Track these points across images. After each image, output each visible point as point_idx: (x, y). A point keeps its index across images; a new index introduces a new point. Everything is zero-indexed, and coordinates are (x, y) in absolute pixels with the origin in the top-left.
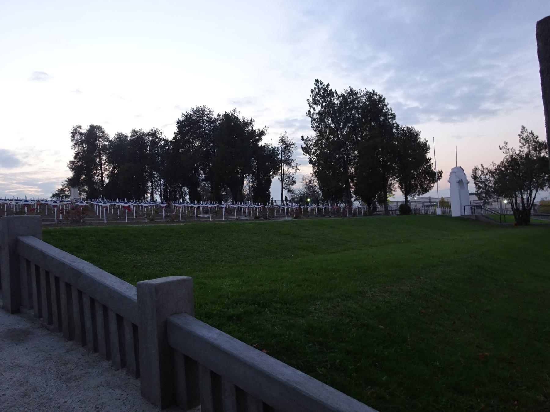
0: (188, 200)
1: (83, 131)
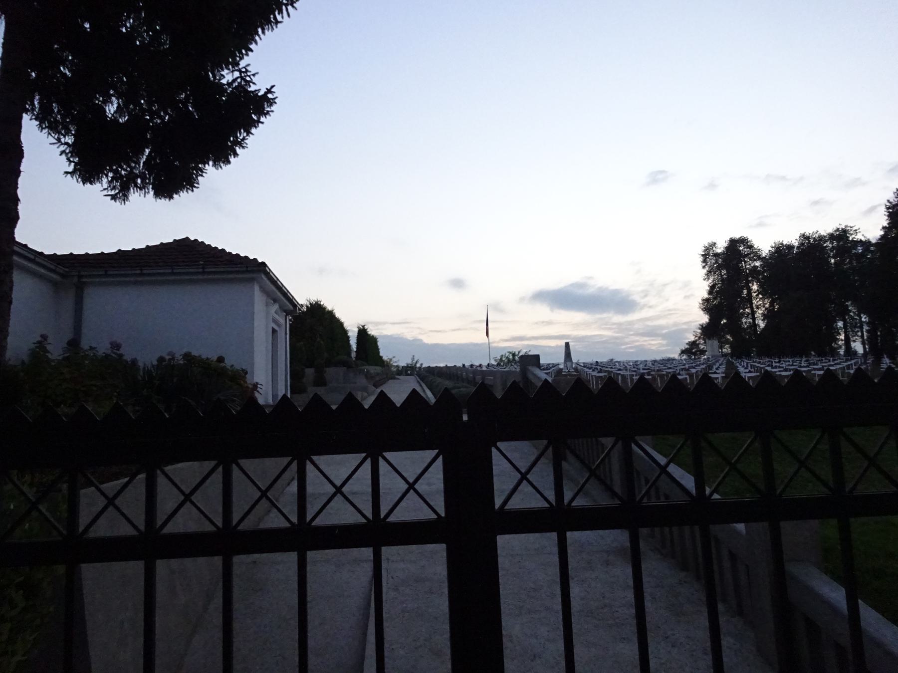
1: (719, 251)
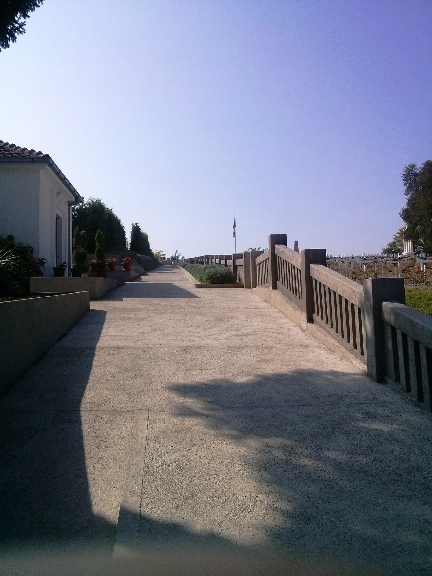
1: (417, 171)
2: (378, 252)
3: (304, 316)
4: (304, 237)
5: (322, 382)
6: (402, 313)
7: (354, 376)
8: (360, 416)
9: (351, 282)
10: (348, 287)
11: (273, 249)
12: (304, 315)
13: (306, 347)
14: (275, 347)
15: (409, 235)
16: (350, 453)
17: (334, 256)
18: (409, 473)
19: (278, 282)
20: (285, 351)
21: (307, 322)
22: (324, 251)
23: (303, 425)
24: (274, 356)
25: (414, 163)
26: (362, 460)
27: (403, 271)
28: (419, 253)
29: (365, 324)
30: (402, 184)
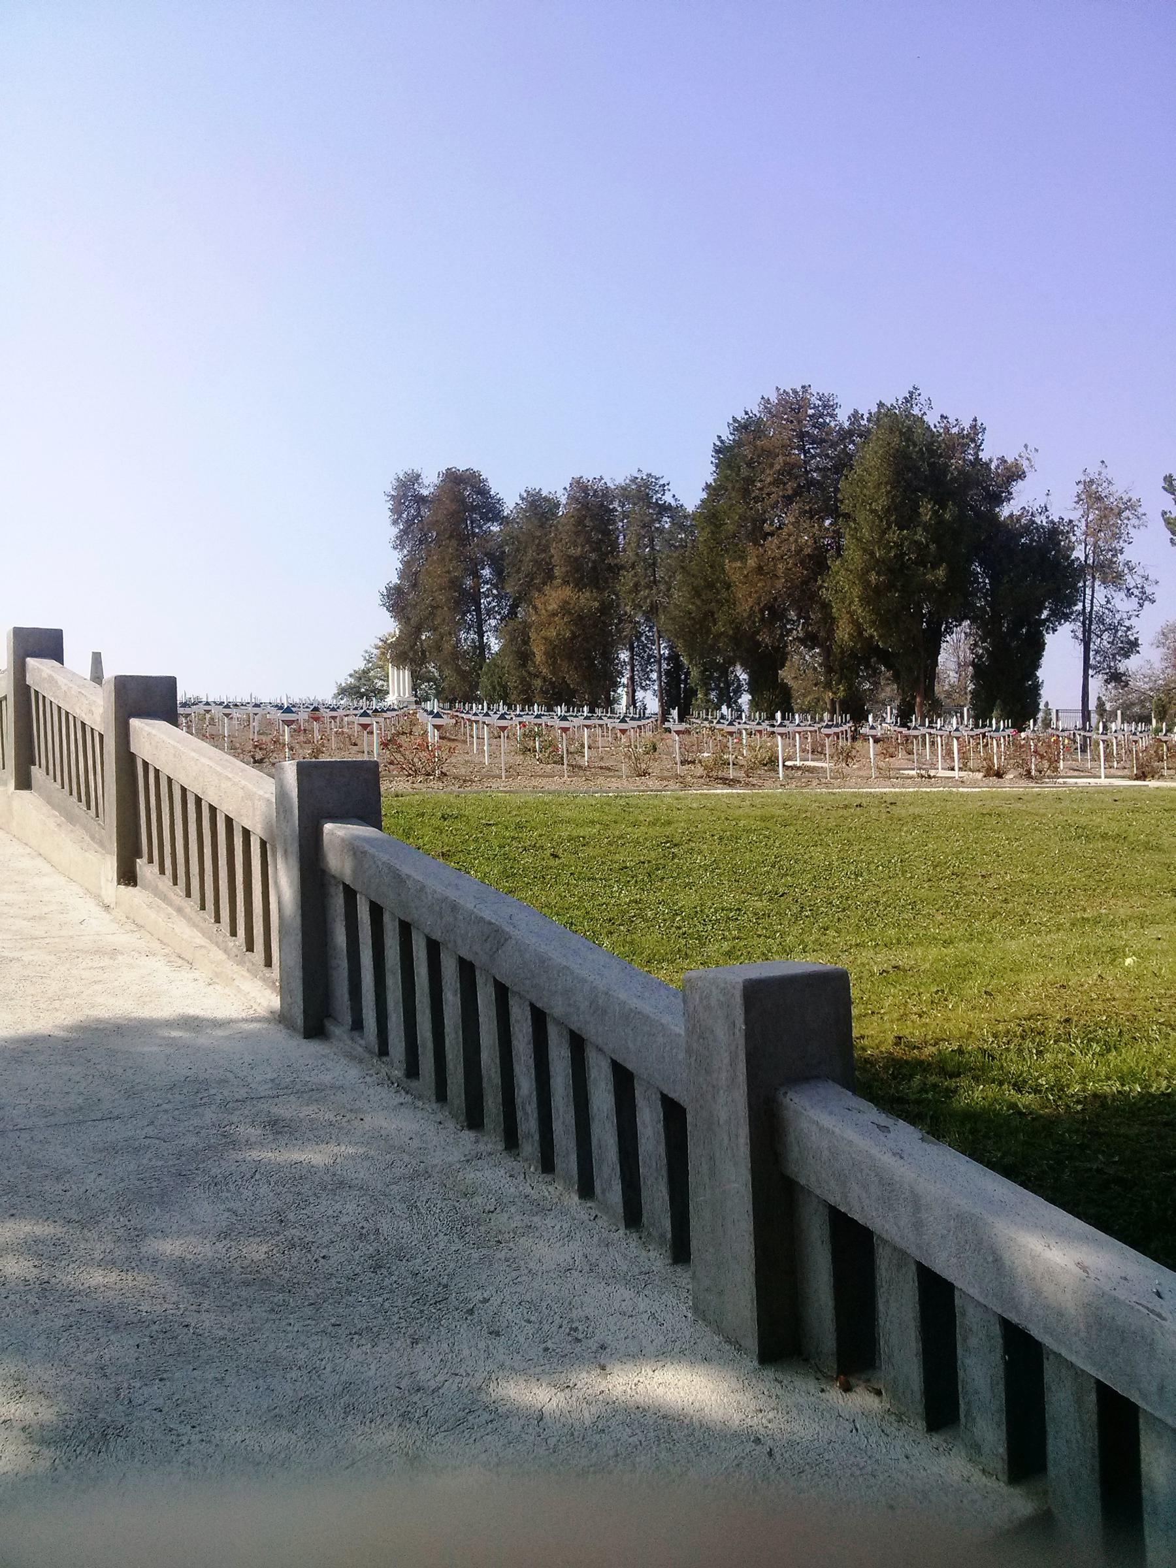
0: (745, 707)
1: (425, 492)
2: (324, 692)
3: (110, 866)
4: (112, 638)
5: (155, 1049)
6: (372, 851)
7: (246, 1026)
8: (255, 1133)
9: (243, 770)
10: (235, 784)
11: (20, 670)
12: (109, 863)
13: (114, 952)
14: (18, 959)
15: (404, 652)
16: (224, 1235)
17: (204, 700)
18: (376, 1268)
19: (34, 769)
20: (47, 969)
21: (119, 884)
22: (170, 684)
23: (93, 1176)
24: (13, 987)
25: (417, 470)
26: (256, 1251)
27: (384, 745)
28: (427, 699)
29: (276, 883)
30: (389, 521)
